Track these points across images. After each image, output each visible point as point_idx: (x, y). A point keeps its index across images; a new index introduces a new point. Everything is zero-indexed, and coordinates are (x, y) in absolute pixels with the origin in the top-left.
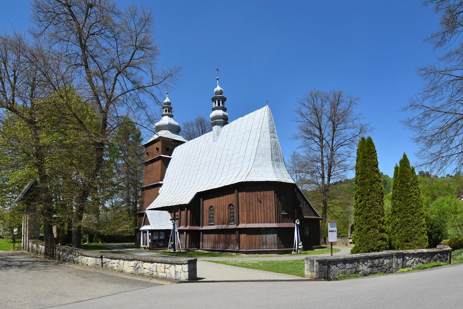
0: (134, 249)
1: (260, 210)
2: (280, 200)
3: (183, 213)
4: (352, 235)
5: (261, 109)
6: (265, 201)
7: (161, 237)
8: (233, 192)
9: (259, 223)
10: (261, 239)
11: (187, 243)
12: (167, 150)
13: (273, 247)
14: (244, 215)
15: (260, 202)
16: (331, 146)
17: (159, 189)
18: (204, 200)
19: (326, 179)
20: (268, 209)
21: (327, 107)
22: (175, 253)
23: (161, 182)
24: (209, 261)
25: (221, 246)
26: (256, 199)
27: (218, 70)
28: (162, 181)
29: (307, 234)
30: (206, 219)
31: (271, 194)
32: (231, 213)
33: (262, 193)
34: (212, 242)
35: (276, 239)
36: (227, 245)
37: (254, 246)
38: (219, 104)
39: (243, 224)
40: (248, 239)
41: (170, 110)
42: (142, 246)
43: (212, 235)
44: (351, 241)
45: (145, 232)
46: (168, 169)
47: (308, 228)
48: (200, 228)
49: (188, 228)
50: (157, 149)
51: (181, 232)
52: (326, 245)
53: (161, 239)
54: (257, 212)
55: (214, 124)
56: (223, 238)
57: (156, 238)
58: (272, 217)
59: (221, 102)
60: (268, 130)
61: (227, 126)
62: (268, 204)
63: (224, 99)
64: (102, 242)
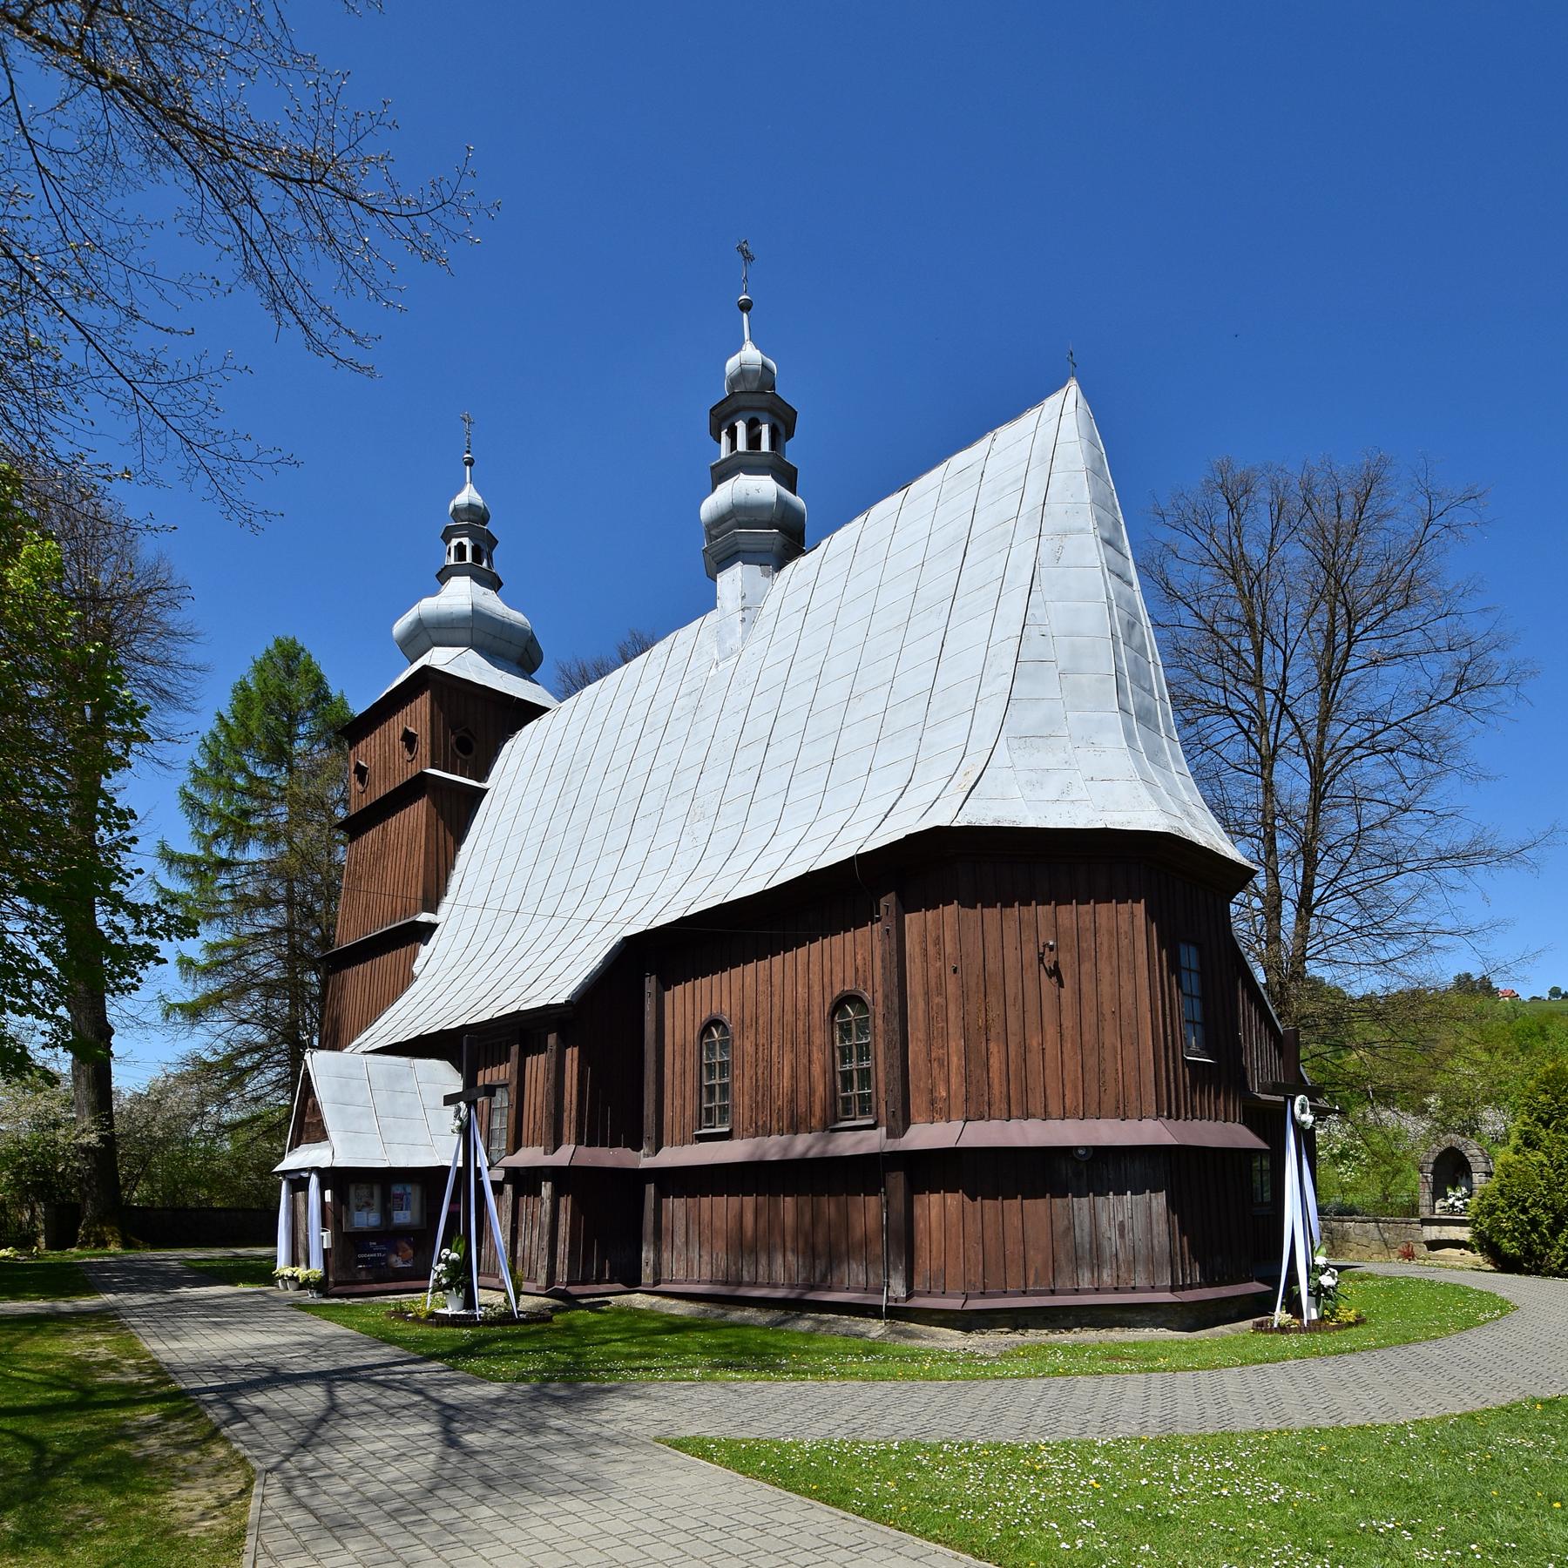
0: (241, 1288)
1: (1051, 1031)
2: (1175, 966)
3: (538, 1065)
5: (1029, 419)
6: (1087, 967)
7: (402, 1217)
8: (860, 917)
9: (1046, 1117)
10: (1061, 1225)
11: (562, 1248)
12: (464, 746)
13: (1141, 1281)
14: (944, 1063)
15: (1055, 972)
17: (415, 955)
18: (666, 984)
20: (1109, 1026)
21: (1296, 555)
23: (424, 917)
24: (743, 1458)
25: (780, 1273)
26: (1030, 952)
27: (748, 258)
28: (434, 910)
30: (679, 1099)
31: (1126, 923)
32: (846, 1055)
33: (1067, 913)
34: (720, 1244)
35: (1161, 1227)
36: (821, 1266)
37: (1014, 1273)
38: (754, 442)
39: (940, 1126)
40: (973, 1228)
41: (485, 546)
42: (283, 1267)
43: (721, 1201)
45: (298, 1182)
46: (466, 848)
48: (645, 1160)
49: (563, 1156)
50: (409, 739)
51: (523, 1181)
53: (391, 1224)
54: (1034, 1042)
55: (723, 561)
56: (789, 1219)
57: (367, 1219)
60: (1087, 520)
61: (803, 561)
62: (1105, 988)
63: (785, 424)
64: (127, 1244)
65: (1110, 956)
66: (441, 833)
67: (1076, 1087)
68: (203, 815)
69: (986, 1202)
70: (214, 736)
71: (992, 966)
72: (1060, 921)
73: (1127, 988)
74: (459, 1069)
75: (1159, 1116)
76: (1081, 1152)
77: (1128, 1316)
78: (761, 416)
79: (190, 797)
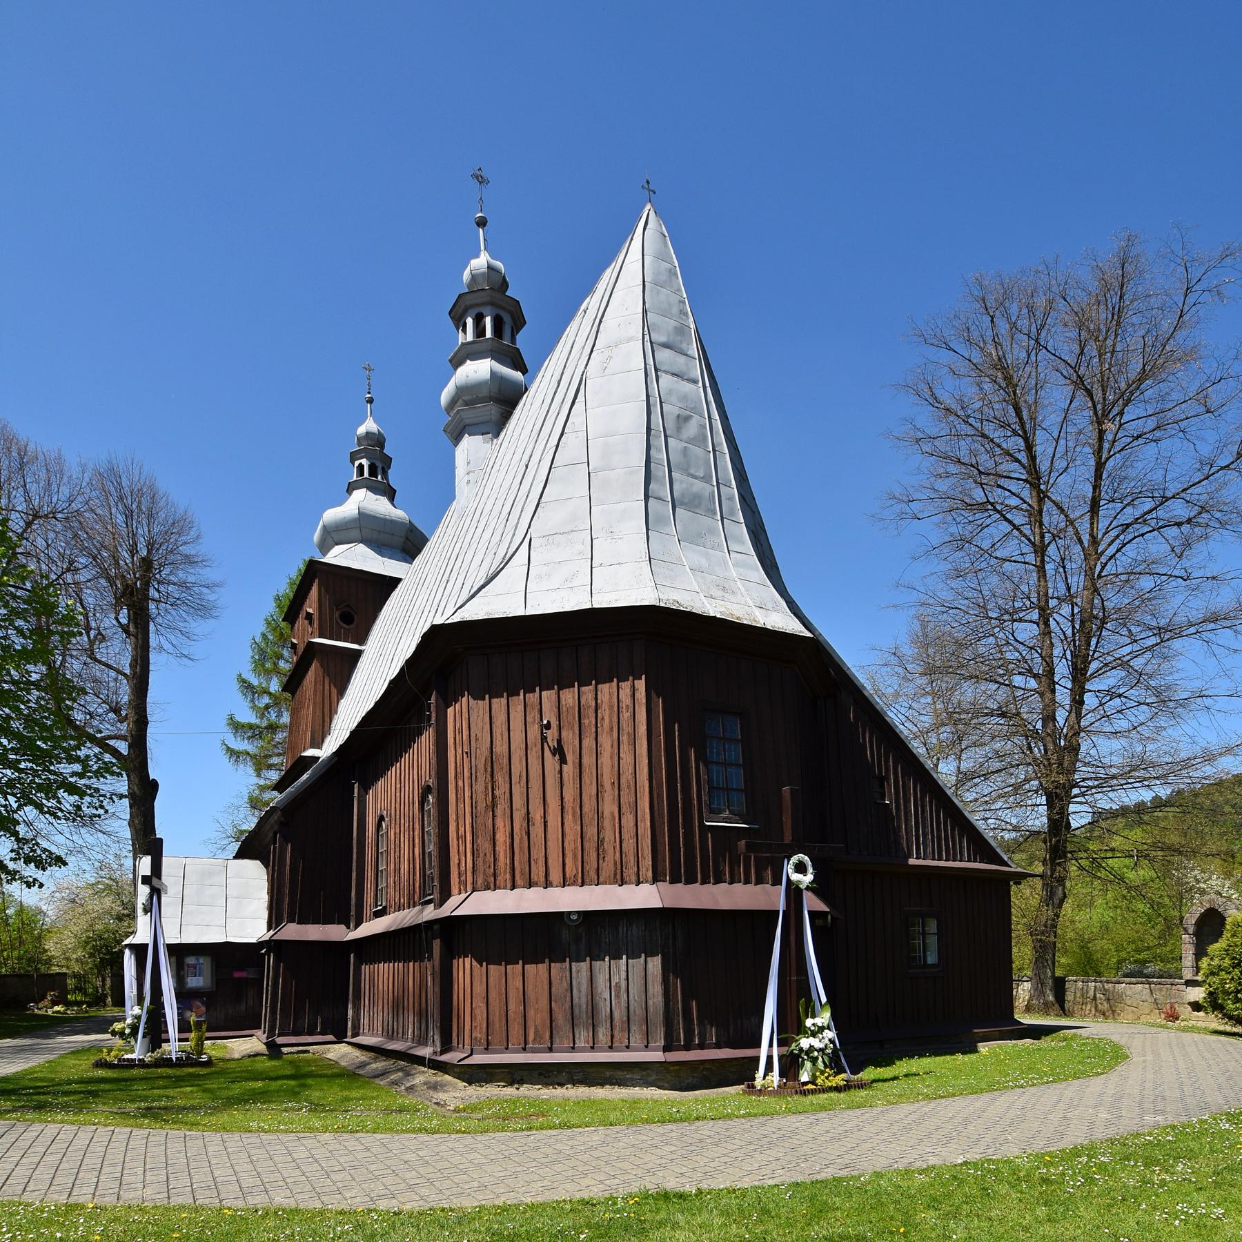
4: (1204, 962)
6: (588, 742)
9: (547, 884)
12: (347, 618)
15: (559, 751)
16: (1086, 538)
19: (1063, 695)
22: (166, 1062)
27: (481, 180)
28: (320, 747)
29: (932, 959)
35: (656, 989)
37: (516, 1030)
38: (480, 331)
44: (1198, 994)
47: (933, 926)
52: (1064, 1013)
54: (537, 815)
58: (629, 845)
59: (488, 321)
62: (605, 760)
65: (611, 729)
66: (327, 687)
67: (575, 856)
68: (254, 693)
69: (491, 967)
70: (264, 636)
71: (501, 748)
72: (563, 702)
73: (627, 758)
74: (266, 867)
75: (655, 880)
76: (574, 917)
77: (619, 1074)
78: (485, 310)
79: (244, 681)
